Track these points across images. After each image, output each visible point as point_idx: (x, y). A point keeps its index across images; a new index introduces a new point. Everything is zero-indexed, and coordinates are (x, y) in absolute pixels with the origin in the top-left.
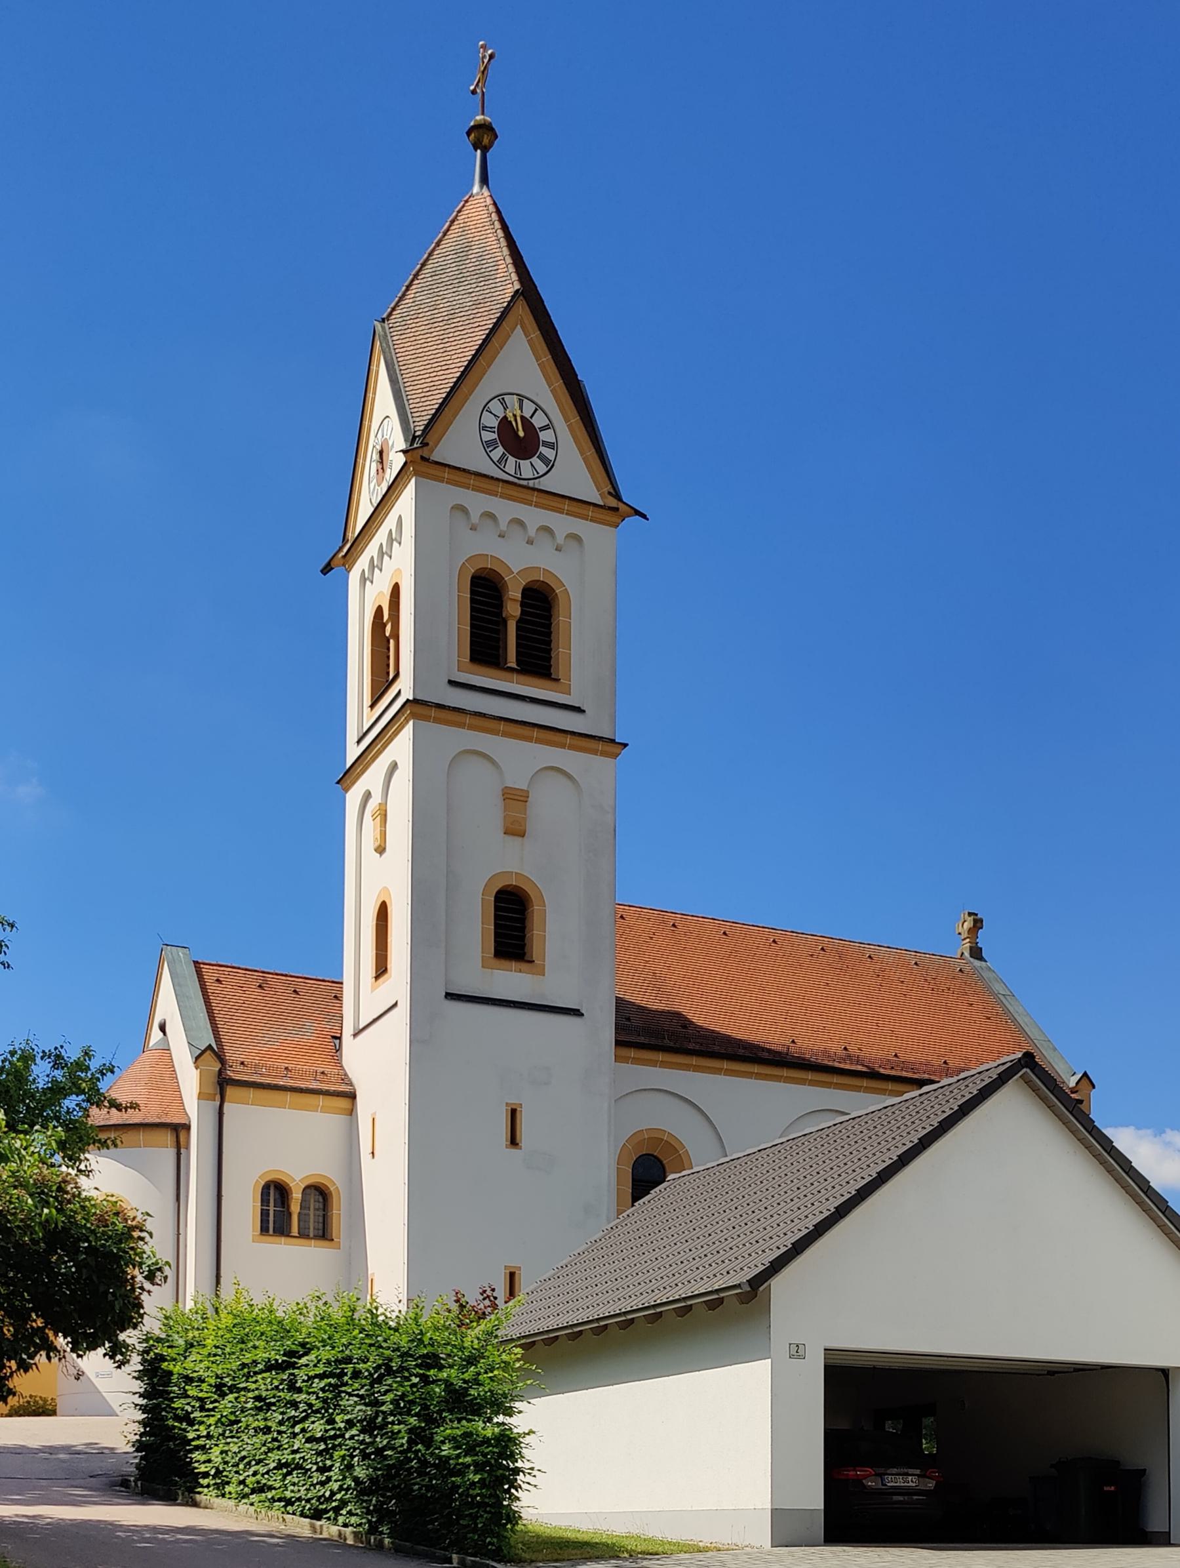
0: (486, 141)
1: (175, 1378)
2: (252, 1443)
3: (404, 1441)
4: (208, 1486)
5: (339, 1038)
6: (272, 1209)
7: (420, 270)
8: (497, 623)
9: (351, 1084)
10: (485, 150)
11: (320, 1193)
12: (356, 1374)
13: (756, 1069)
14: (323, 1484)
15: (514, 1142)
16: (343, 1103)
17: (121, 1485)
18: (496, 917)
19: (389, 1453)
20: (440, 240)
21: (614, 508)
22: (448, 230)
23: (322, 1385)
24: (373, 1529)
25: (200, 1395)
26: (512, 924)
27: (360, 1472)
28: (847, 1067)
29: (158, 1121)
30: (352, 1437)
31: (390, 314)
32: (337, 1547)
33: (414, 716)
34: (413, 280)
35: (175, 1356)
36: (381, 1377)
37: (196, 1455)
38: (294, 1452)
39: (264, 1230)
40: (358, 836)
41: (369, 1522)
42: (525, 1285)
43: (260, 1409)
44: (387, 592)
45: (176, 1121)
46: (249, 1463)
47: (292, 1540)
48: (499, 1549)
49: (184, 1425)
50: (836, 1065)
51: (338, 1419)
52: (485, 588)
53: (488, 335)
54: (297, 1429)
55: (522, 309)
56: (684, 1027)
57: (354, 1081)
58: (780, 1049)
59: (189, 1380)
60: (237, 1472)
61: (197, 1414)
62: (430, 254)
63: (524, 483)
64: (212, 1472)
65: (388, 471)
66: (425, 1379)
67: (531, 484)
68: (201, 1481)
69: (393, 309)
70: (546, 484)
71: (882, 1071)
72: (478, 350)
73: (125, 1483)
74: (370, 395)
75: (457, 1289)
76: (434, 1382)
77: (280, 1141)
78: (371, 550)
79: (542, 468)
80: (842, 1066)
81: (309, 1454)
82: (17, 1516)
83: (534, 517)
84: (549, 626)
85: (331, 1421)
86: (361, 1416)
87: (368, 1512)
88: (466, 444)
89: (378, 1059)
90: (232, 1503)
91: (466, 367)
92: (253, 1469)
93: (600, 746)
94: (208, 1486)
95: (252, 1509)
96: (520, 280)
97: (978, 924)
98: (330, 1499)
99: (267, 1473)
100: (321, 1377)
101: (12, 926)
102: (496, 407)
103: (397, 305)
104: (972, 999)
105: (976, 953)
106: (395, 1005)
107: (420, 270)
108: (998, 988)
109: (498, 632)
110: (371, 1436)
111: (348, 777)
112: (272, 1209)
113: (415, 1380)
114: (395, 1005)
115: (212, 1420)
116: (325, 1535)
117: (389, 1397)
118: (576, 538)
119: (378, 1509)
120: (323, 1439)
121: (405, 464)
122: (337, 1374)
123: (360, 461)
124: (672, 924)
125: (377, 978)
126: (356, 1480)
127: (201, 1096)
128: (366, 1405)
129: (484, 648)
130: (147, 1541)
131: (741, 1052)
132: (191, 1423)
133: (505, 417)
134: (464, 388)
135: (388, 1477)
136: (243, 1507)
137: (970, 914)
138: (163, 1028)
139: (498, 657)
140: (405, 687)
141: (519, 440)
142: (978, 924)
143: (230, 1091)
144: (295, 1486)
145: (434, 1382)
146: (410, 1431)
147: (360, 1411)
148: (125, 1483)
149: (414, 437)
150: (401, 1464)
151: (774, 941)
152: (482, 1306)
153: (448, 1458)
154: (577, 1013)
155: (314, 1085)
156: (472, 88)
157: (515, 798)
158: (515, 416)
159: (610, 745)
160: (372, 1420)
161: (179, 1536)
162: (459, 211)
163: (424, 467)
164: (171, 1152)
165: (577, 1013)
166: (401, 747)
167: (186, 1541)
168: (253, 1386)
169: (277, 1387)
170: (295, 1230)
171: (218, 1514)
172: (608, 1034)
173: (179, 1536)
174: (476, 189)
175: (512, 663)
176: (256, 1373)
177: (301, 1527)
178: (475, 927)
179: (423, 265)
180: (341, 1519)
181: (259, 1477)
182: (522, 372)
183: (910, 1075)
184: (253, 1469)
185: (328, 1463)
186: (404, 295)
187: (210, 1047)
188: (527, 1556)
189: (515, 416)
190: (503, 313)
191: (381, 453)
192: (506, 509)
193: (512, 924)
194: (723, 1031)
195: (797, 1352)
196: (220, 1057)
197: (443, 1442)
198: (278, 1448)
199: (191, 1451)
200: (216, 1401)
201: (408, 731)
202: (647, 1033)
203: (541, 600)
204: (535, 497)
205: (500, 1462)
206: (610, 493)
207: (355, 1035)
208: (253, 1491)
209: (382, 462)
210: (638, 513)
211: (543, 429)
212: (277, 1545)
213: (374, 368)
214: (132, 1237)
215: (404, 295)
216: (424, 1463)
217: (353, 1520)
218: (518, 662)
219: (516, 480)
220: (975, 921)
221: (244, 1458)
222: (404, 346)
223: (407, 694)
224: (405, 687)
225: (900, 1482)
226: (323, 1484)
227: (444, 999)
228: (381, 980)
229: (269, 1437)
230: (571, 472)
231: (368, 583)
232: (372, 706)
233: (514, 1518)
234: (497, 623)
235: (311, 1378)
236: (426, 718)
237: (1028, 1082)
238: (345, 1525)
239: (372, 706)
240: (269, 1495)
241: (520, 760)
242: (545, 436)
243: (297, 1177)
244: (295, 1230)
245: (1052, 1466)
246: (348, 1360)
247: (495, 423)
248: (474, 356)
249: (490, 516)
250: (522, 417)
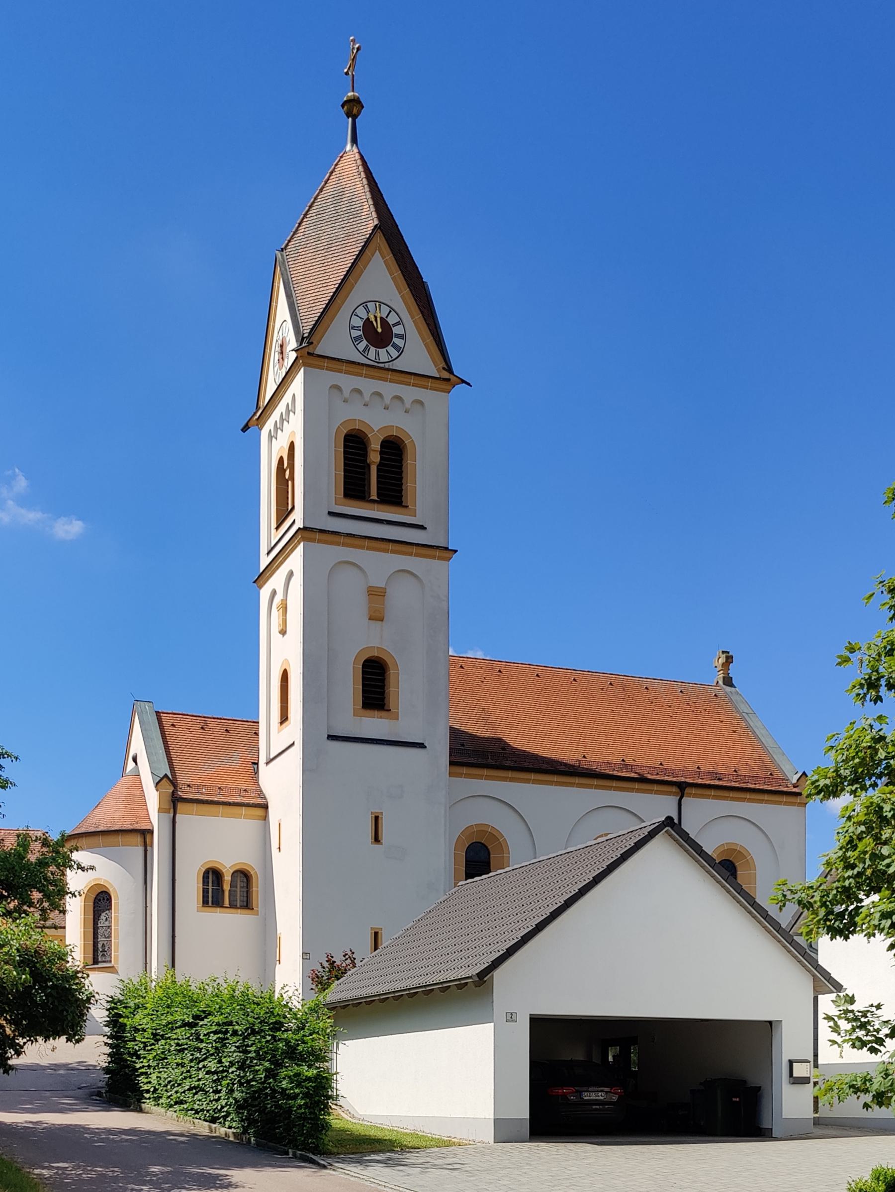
0: (355, 111)
1: (128, 1028)
2: (175, 1073)
3: (263, 1076)
4: (149, 1098)
5: (257, 764)
6: (210, 888)
7: (308, 210)
8: (363, 468)
9: (265, 798)
10: (354, 118)
11: (243, 876)
12: (235, 1033)
13: (555, 778)
14: (217, 1100)
15: (377, 839)
16: (259, 812)
17: (96, 1096)
18: (363, 678)
19: (254, 1083)
20: (323, 188)
21: (447, 378)
22: (328, 179)
23: (215, 1038)
24: (245, 1131)
25: (143, 1040)
26: (375, 684)
27: (237, 1095)
28: (623, 774)
29: (132, 828)
30: (232, 1072)
31: (287, 245)
32: (220, 1143)
33: (304, 539)
34: (303, 219)
35: (128, 1014)
36: (249, 1034)
37: (142, 1079)
38: (199, 1080)
39: (205, 902)
40: (268, 622)
41: (243, 1126)
42: (385, 942)
43: (179, 1051)
44: (286, 447)
45: (144, 827)
46: (173, 1085)
47: (194, 1137)
48: (317, 1146)
49: (134, 1059)
50: (615, 773)
51: (224, 1060)
52: (354, 443)
53: (355, 260)
54: (201, 1066)
55: (380, 239)
56: (504, 749)
57: (267, 796)
58: (571, 763)
59: (137, 1030)
60: (166, 1091)
61: (141, 1052)
62: (316, 198)
63: (382, 365)
64: (152, 1090)
65: (286, 360)
66: (274, 1037)
67: (387, 365)
68: (145, 1095)
69: (289, 241)
70: (398, 365)
71: (649, 777)
72: (348, 271)
73: (99, 1094)
74: (274, 304)
75: (329, 952)
76: (279, 1040)
77: (215, 840)
78: (275, 416)
79: (394, 353)
80: (619, 774)
81: (207, 1081)
82: (26, 1122)
83: (390, 389)
84: (401, 467)
85: (220, 1062)
86: (238, 1059)
87: (242, 1120)
88: (340, 341)
89: (282, 781)
90: (163, 1110)
91: (340, 284)
92: (175, 1089)
93: (437, 553)
94: (149, 1098)
95: (175, 1114)
96: (379, 217)
97: (729, 659)
98: (220, 1111)
99: (184, 1092)
100: (215, 1033)
101: (17, 758)
102: (361, 312)
103: (292, 238)
104: (723, 717)
105: (728, 681)
106: (293, 744)
107: (308, 210)
108: (743, 708)
109: (364, 474)
110: (244, 1071)
111: (261, 578)
112: (210, 888)
113: (269, 1038)
114: (293, 744)
115: (150, 1057)
116: (217, 1134)
117: (253, 1048)
118: (421, 403)
119: (247, 1119)
120: (215, 1072)
121: (297, 358)
122: (224, 1030)
123: (268, 351)
124: (498, 669)
125: (281, 723)
126: (235, 1099)
127: (160, 810)
128: (240, 1052)
129: (354, 488)
130: (102, 1140)
131: (545, 766)
132: (139, 1057)
133: (368, 319)
134: (338, 301)
135: (253, 1098)
136: (170, 1113)
137: (723, 652)
138: (135, 760)
139: (364, 492)
140: (298, 518)
141: (378, 335)
142: (729, 659)
143: (180, 806)
144: (200, 1101)
145: (279, 1040)
146: (266, 1070)
147: (237, 1056)
148: (99, 1094)
149: (303, 338)
150: (260, 1091)
151: (574, 680)
152: (344, 965)
153: (286, 1089)
154: (421, 746)
155: (239, 800)
156: (346, 70)
157: (376, 594)
158: (376, 317)
159: (445, 552)
160: (245, 1061)
161: (124, 1137)
162: (336, 165)
163: (311, 360)
164: (141, 849)
165: (421, 746)
166: (296, 561)
167: (127, 1140)
168: (175, 1036)
169: (188, 1038)
170: (227, 903)
171: (155, 1119)
172: (445, 759)
173: (124, 1137)
174: (348, 147)
175: (374, 496)
176: (177, 1028)
177: (202, 1128)
178: (349, 687)
179: (311, 207)
180: (227, 1124)
181: (179, 1095)
182: (381, 285)
183: (670, 779)
184: (175, 1089)
185: (219, 1088)
186: (297, 230)
187: (166, 776)
188: (335, 1150)
189: (376, 317)
190: (366, 242)
191: (282, 346)
192: (368, 385)
193: (375, 684)
194: (532, 751)
195: (511, 1017)
196: (174, 783)
197: (284, 1078)
198: (190, 1077)
199: (139, 1076)
200: (153, 1044)
201: (300, 550)
202: (476, 755)
203: (394, 449)
204: (389, 375)
205: (320, 1091)
206: (444, 368)
207: (267, 763)
208: (176, 1103)
209: (282, 353)
210: (463, 381)
211: (395, 325)
212: (183, 1142)
213: (276, 284)
214: (78, 977)
215: (297, 230)
216: (274, 1091)
217: (234, 1124)
218: (379, 495)
219: (376, 364)
220: (727, 658)
221: (170, 1082)
222: (296, 270)
223: (299, 524)
224: (298, 518)
225: (593, 1096)
226: (217, 1100)
227: (326, 740)
228: (284, 725)
229: (184, 1070)
230: (416, 354)
231: (274, 439)
232: (277, 528)
233: (326, 1126)
234: (363, 468)
235: (208, 1034)
236: (312, 540)
237: (671, 835)
238: (230, 1127)
239: (277, 528)
240: (185, 1106)
241: (379, 566)
242: (396, 330)
243: (227, 867)
244: (227, 903)
245: (701, 1084)
246: (230, 1023)
247: (360, 323)
248: (345, 276)
249: (358, 391)
250: (381, 318)
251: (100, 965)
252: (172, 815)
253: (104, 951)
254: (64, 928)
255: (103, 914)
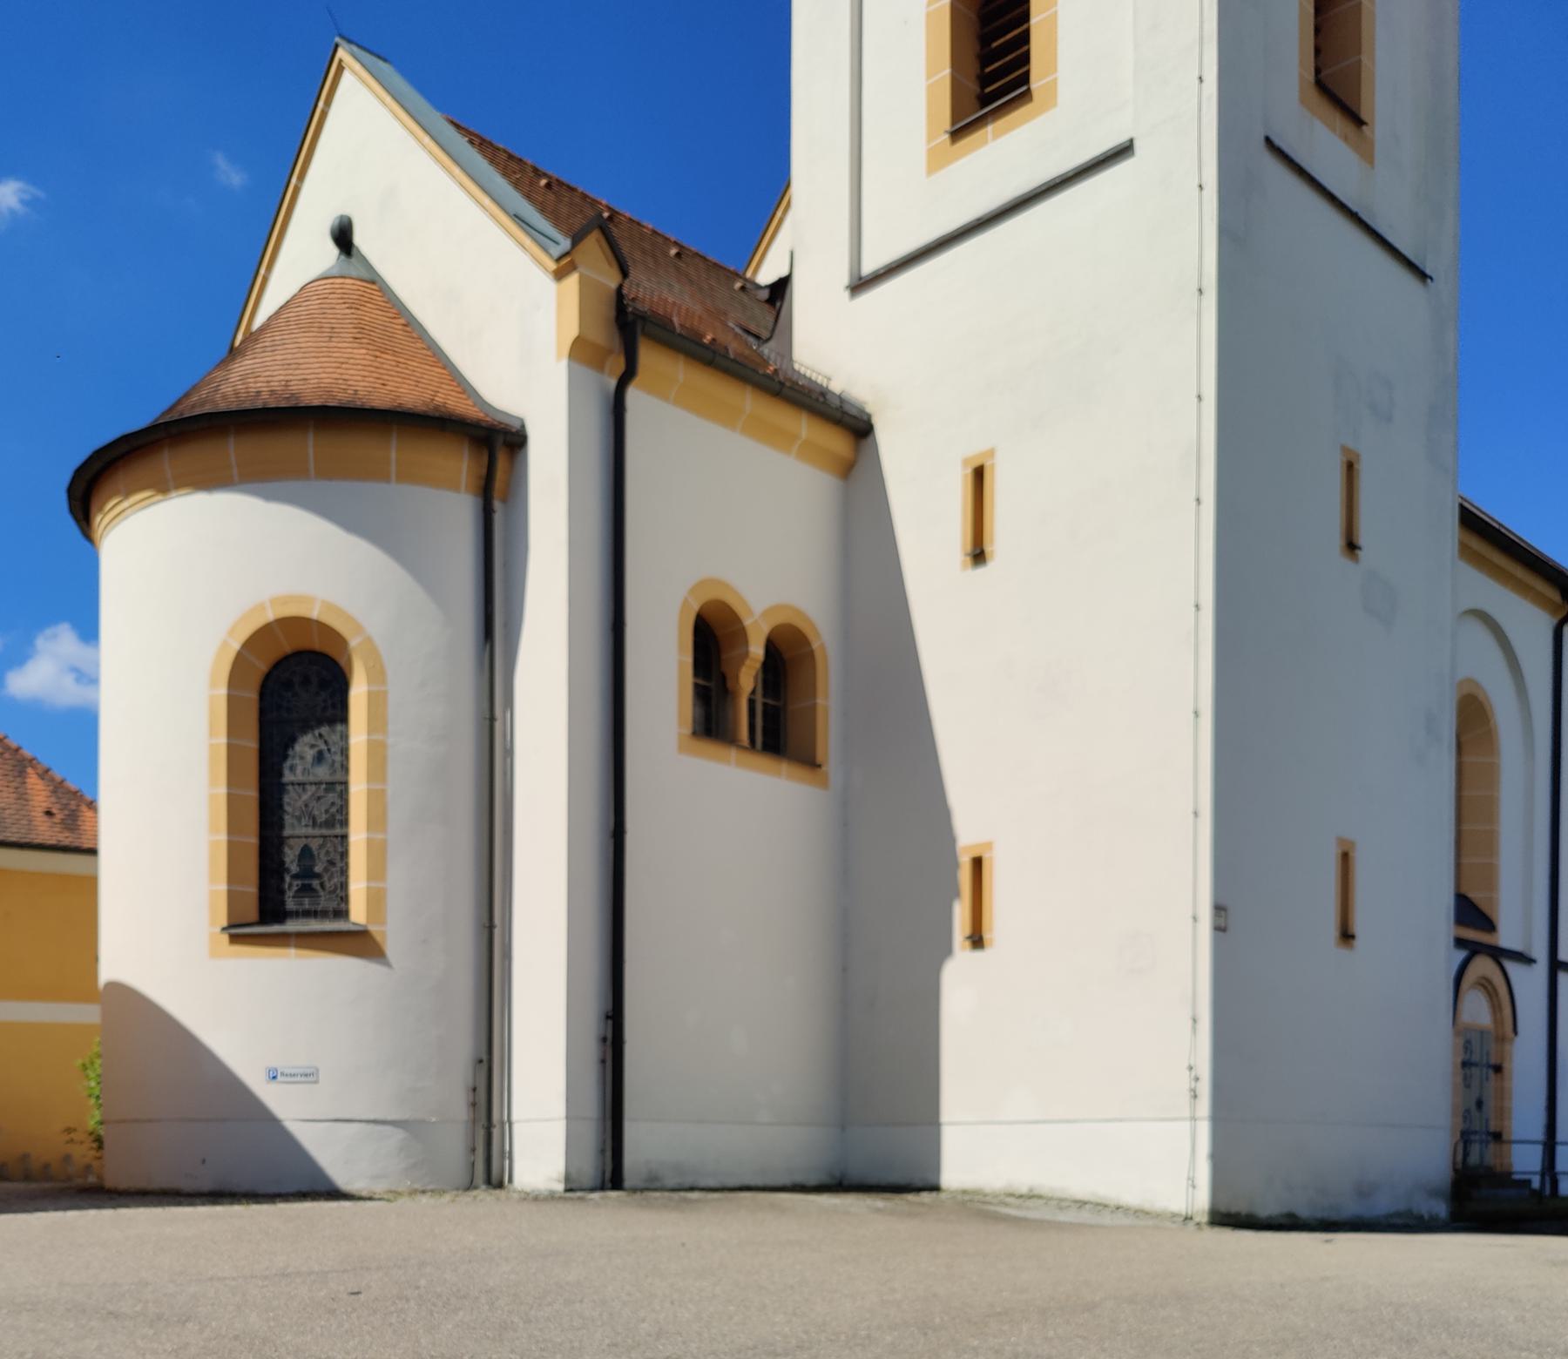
11: (787, 659)
143: (650, 357)
251: (291, 926)
252: (612, 383)
253: (307, 873)
254: (93, 852)
255: (308, 738)
